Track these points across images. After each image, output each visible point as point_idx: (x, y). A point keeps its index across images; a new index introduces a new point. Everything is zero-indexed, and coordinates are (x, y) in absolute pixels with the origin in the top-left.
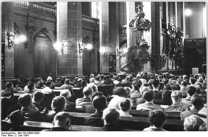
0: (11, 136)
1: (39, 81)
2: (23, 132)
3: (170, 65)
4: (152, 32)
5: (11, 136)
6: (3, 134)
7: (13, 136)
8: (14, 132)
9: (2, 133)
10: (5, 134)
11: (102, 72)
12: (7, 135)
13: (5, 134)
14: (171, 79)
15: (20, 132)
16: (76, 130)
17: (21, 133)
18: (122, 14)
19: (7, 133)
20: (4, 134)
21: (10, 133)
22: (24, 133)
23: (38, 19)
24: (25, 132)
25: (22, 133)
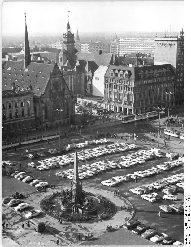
0: (189, 204)
1: (179, 157)
2: (185, 219)
3: (61, 61)
4: (20, 51)
5: (189, 204)
6: (187, 244)
7: (189, 222)
8: (185, 231)
9: (186, 245)
10: (188, 241)
11: (161, 140)
12: (188, 232)
13: (188, 241)
14: (25, 55)
15: (185, 223)
16: (167, 217)
17: (186, 222)
18: (87, 98)
19: (186, 238)
20: (188, 243)
21: (187, 235)
22: (186, 218)
23: (91, 195)
24: (185, 218)
25: (186, 221)
